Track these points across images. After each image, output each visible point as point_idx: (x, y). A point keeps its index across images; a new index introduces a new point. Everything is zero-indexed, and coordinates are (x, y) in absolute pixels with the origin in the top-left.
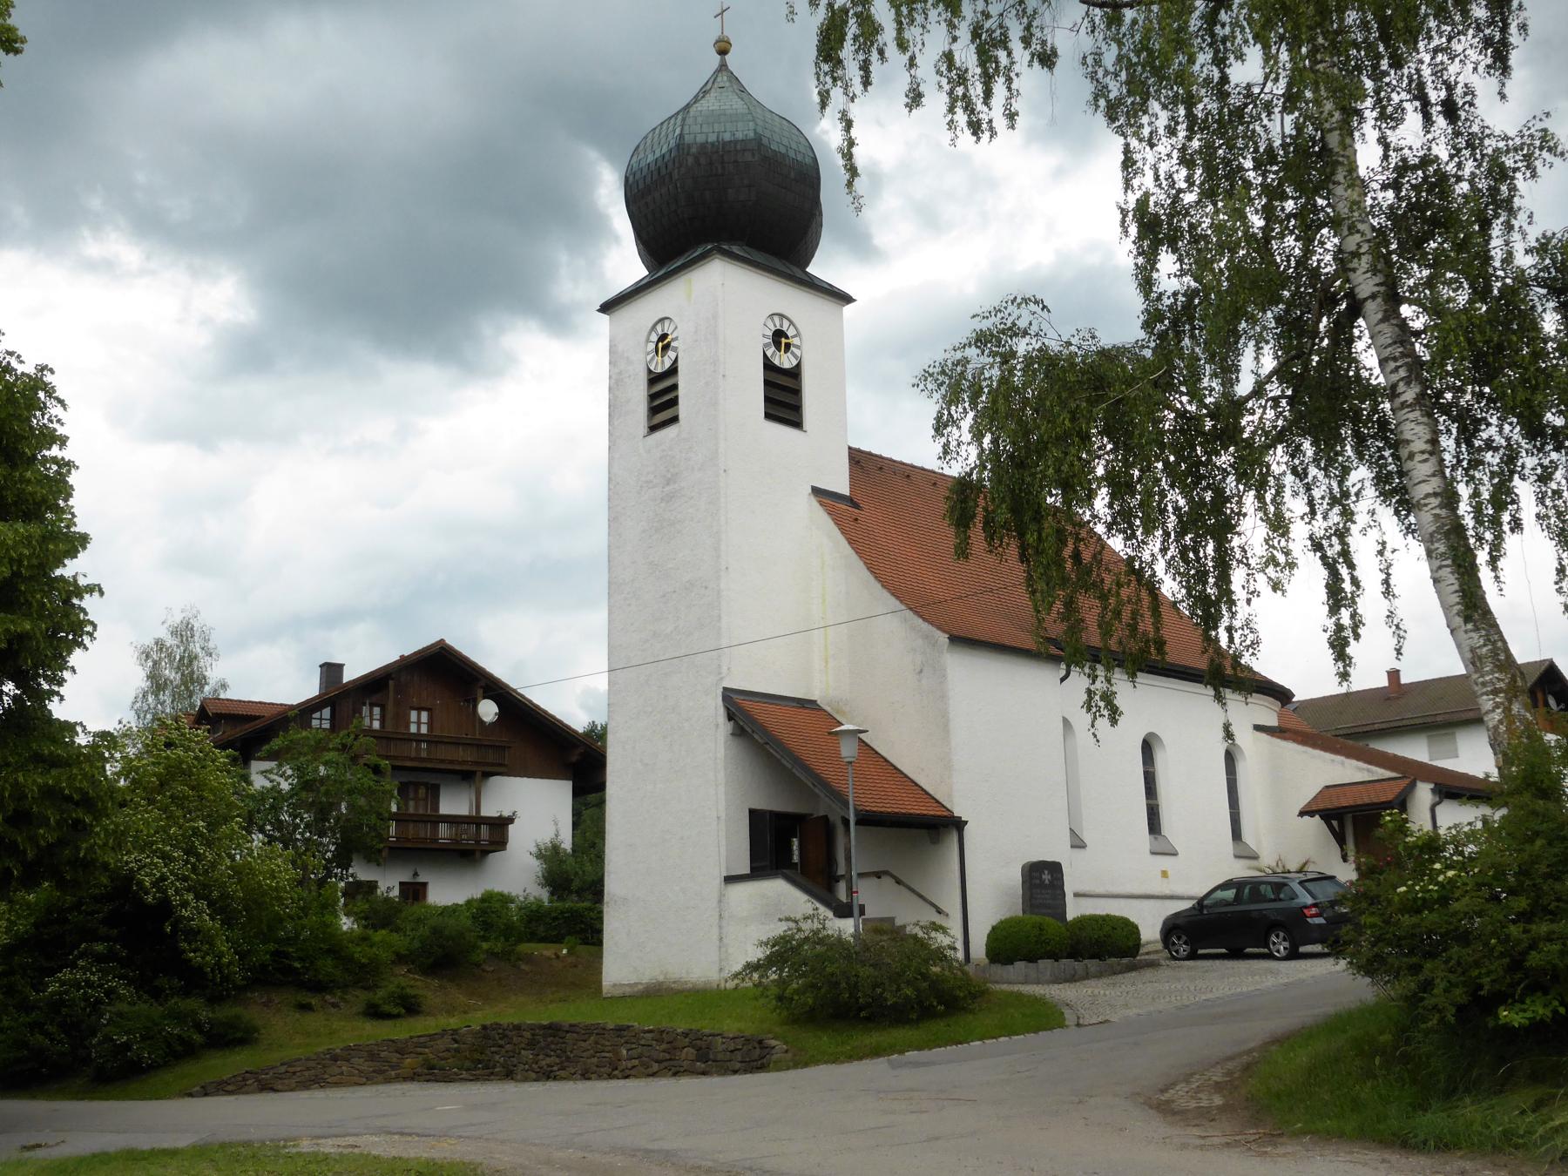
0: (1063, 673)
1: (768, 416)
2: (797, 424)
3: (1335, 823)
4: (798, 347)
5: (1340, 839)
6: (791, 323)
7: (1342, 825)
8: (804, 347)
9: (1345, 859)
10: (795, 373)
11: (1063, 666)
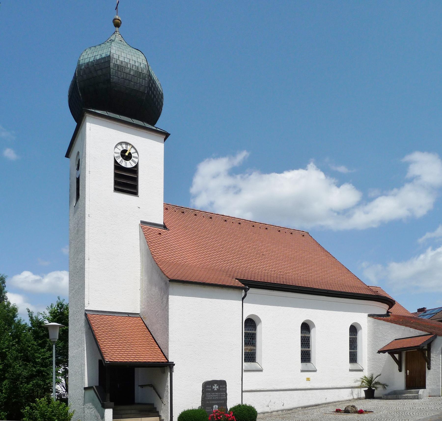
0: (243, 295)
1: (116, 190)
2: (135, 193)
3: (397, 356)
4: (136, 158)
5: (399, 363)
6: (133, 147)
7: (400, 357)
8: (140, 158)
9: (400, 370)
10: (135, 170)
11: (243, 291)
